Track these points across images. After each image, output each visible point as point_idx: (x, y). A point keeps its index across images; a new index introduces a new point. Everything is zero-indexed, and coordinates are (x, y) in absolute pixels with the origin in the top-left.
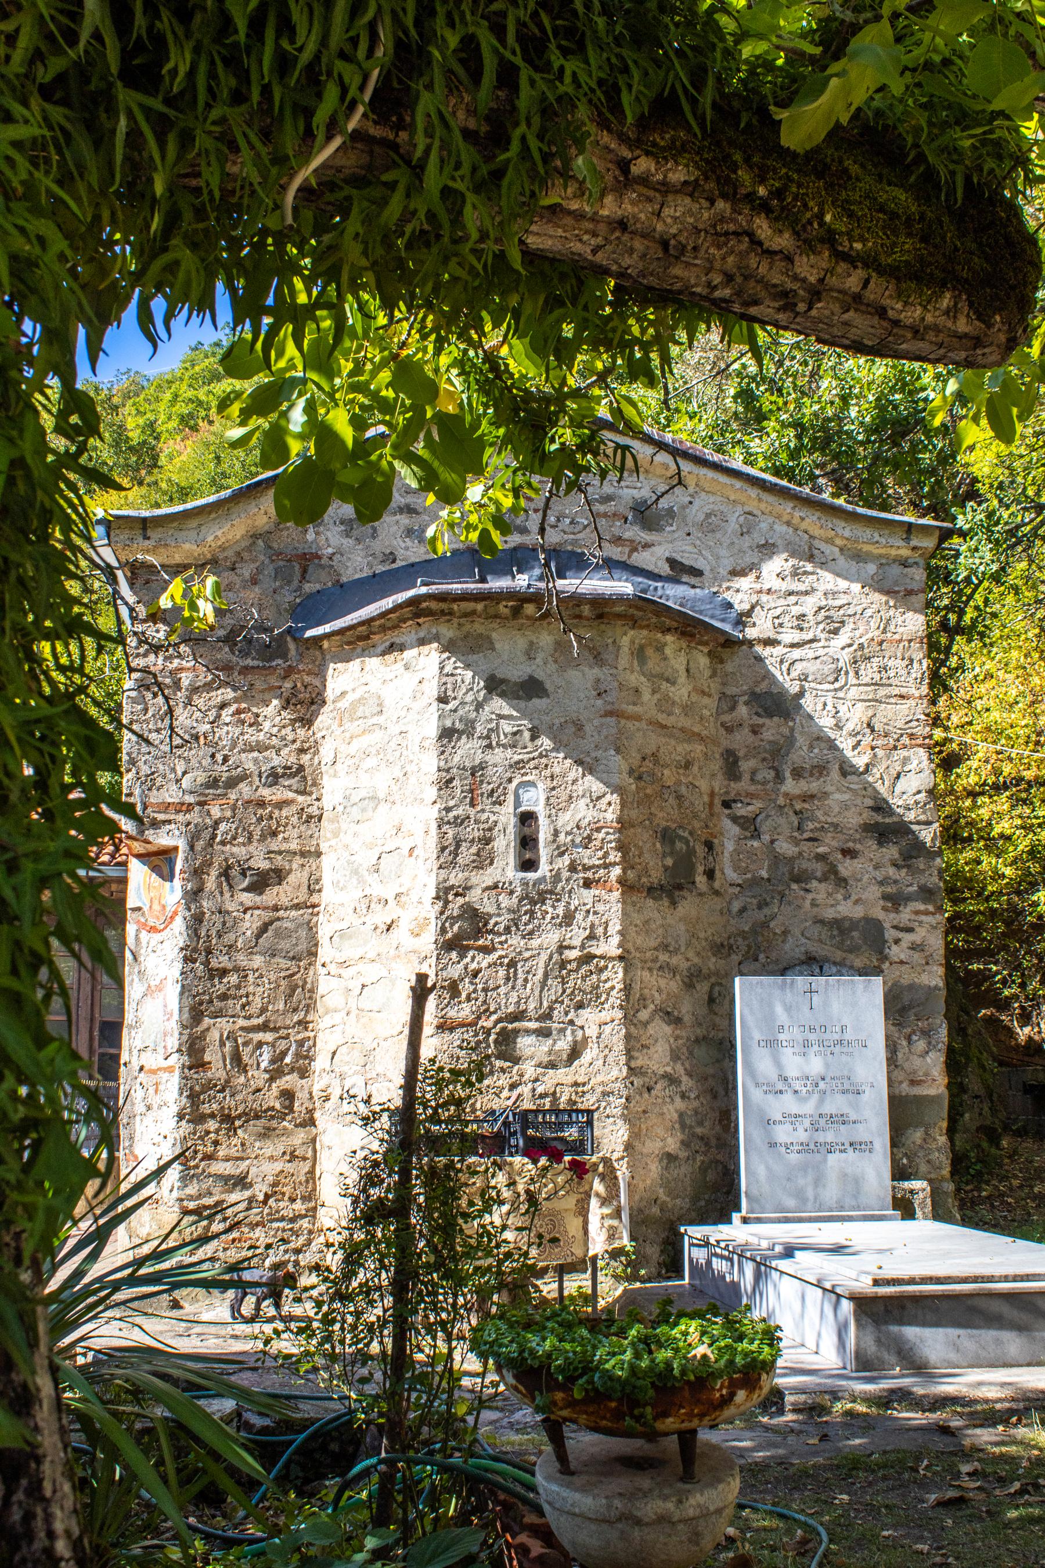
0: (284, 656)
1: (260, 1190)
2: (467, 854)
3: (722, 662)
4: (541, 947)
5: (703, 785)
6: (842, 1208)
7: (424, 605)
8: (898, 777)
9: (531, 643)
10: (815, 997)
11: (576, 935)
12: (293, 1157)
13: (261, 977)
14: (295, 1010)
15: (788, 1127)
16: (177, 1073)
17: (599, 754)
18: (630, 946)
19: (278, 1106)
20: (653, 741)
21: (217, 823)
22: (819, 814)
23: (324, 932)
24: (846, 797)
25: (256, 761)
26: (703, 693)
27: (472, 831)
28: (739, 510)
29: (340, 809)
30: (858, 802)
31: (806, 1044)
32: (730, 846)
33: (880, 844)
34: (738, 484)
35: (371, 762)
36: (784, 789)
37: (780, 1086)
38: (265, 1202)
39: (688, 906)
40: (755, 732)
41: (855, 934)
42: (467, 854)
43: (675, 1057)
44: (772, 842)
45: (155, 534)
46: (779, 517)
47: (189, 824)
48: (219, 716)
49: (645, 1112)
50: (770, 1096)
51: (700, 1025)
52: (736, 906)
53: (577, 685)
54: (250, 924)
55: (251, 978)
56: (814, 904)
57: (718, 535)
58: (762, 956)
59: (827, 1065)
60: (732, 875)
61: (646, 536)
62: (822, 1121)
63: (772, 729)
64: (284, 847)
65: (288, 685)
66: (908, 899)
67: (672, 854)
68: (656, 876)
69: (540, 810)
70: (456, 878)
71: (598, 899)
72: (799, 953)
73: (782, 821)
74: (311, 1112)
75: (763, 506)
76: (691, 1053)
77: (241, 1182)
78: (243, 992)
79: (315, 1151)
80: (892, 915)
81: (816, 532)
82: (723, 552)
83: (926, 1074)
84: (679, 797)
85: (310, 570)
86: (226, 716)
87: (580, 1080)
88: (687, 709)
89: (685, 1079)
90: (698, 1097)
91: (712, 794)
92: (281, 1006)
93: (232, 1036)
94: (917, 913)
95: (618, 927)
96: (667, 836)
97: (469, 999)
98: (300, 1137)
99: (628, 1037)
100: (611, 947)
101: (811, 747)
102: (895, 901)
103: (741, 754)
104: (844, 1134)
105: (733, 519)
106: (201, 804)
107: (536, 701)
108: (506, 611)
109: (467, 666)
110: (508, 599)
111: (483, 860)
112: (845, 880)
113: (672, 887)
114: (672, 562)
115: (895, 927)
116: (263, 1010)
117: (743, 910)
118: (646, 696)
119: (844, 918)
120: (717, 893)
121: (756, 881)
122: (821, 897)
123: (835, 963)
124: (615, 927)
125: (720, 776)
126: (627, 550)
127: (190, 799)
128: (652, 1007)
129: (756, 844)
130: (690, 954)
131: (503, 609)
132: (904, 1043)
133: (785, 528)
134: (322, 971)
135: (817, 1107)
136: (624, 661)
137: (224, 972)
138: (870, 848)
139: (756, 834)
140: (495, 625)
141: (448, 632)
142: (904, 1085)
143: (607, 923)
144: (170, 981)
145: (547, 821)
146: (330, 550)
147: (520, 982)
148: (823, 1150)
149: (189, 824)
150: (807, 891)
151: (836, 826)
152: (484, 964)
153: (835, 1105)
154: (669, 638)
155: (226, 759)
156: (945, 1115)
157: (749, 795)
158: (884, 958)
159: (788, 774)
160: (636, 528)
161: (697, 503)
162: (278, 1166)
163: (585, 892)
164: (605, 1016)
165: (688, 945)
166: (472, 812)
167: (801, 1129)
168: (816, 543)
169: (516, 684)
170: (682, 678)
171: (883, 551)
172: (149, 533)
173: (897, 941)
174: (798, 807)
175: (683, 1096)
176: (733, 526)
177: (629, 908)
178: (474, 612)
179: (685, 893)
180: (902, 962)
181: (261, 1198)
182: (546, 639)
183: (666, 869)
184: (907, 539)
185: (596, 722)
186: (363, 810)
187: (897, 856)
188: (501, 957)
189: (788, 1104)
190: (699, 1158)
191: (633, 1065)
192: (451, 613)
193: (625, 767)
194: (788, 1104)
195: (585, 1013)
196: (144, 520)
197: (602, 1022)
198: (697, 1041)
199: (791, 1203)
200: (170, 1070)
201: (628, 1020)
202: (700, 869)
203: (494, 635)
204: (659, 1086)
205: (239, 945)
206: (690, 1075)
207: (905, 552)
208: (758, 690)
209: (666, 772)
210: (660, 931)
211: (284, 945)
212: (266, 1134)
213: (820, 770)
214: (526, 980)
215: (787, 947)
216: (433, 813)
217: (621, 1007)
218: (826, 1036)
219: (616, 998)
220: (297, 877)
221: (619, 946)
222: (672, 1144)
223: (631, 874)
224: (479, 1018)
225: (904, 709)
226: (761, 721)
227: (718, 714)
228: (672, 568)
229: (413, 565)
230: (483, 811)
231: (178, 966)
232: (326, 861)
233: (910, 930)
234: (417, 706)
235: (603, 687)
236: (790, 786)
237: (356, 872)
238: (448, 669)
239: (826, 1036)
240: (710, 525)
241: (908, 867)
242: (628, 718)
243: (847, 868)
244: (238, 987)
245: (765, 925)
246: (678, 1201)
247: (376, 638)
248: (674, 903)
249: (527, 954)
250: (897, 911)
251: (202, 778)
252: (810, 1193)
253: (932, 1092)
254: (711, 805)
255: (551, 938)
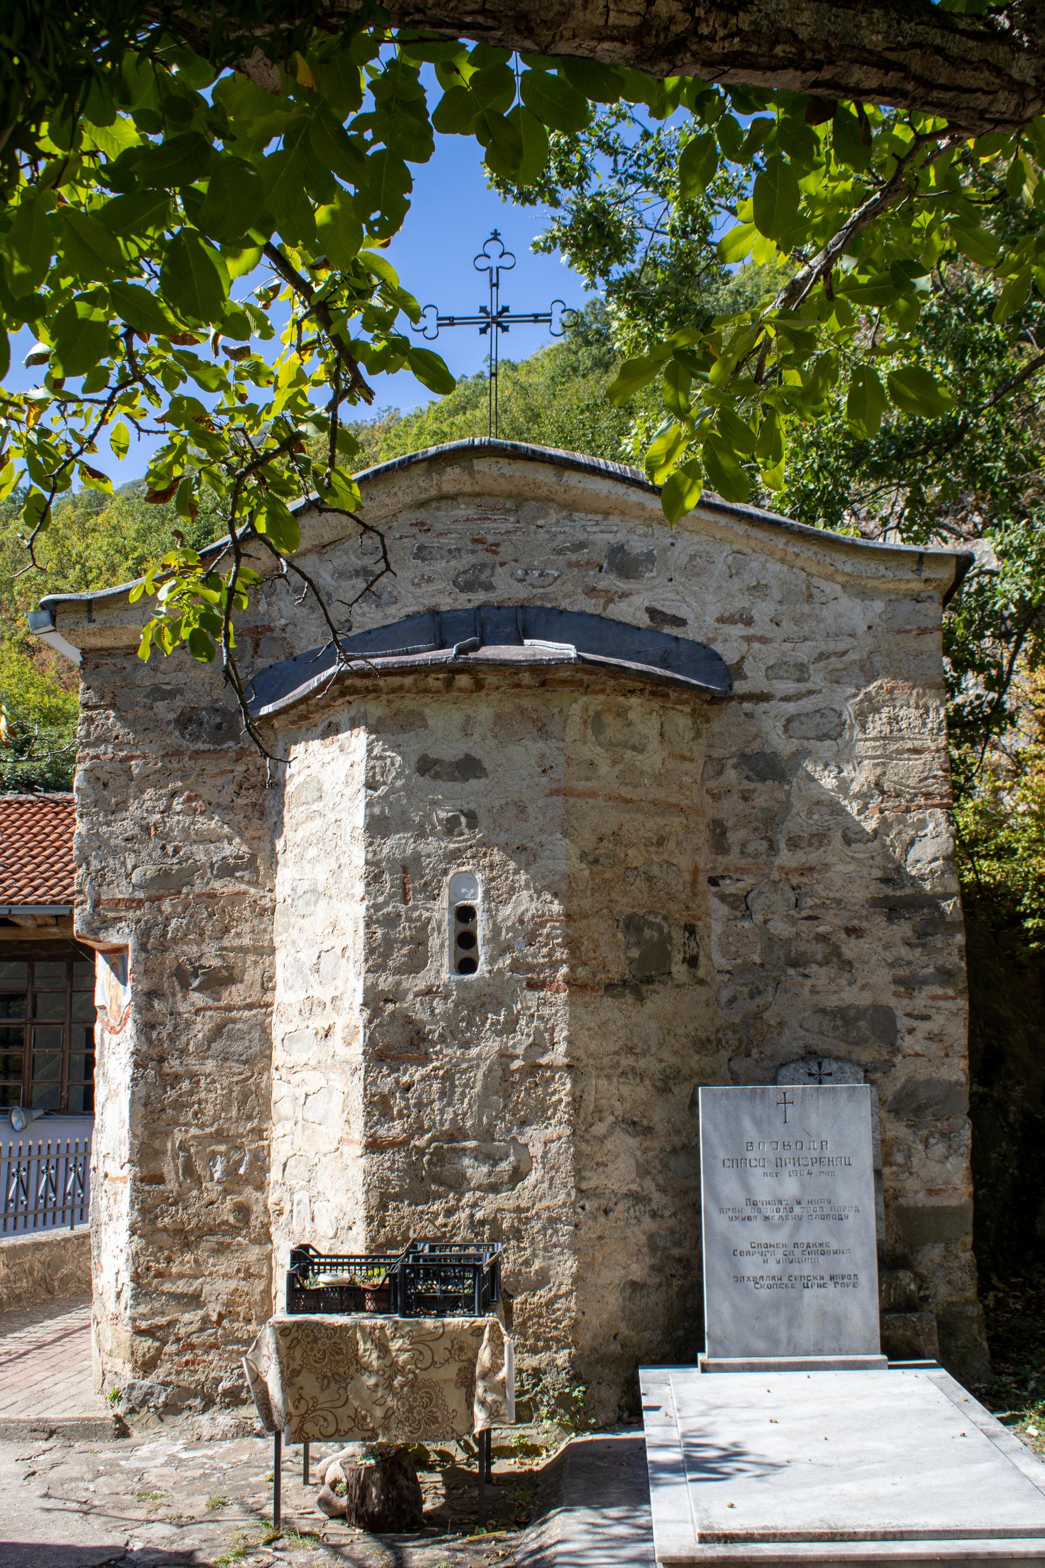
0: (236, 738)
1: (213, 1310)
2: (399, 955)
3: (708, 721)
4: (479, 1056)
5: (684, 862)
6: (820, 1352)
7: (348, 682)
8: (912, 843)
9: (468, 717)
10: (790, 1109)
11: (520, 1041)
12: (249, 1276)
13: (213, 1084)
14: (249, 1118)
15: (757, 1258)
16: (129, 1184)
17: (544, 838)
18: (581, 1053)
19: (232, 1220)
20: (614, 818)
21: (168, 919)
22: (819, 888)
23: (277, 1033)
24: (851, 868)
25: (207, 852)
26: (683, 758)
27: (404, 930)
28: (727, 548)
29: (289, 901)
30: (865, 873)
31: (779, 1163)
32: (717, 928)
33: (890, 920)
34: (723, 520)
35: (312, 852)
36: (778, 861)
37: (748, 1211)
38: (219, 1322)
39: (661, 1000)
40: (745, 799)
41: (862, 1024)
42: (399, 955)
43: (643, 1171)
44: (766, 922)
45: (99, 616)
46: (771, 554)
47: (138, 921)
48: (169, 808)
49: (600, 1238)
50: (736, 1224)
51: (678, 1132)
52: (725, 995)
53: (517, 763)
54: (201, 1028)
55: (202, 1084)
56: (814, 991)
57: (704, 579)
58: (754, 1052)
59: (803, 1187)
60: (720, 961)
61: (623, 585)
62: (797, 1252)
63: (765, 795)
64: (237, 942)
65: (240, 768)
66: (924, 982)
67: (638, 944)
68: (617, 970)
69: (478, 902)
70: (386, 982)
71: (545, 1002)
72: (797, 1047)
73: (777, 898)
74: (266, 1226)
75: (753, 543)
76: (665, 1165)
77: (194, 1300)
78: (195, 1098)
79: (271, 1269)
80: (905, 1002)
81: (814, 569)
82: (710, 598)
83: (947, 1182)
84: (649, 878)
85: (262, 643)
86: (177, 805)
87: (523, 1205)
88: (660, 778)
89: (656, 1196)
90: (675, 1214)
91: (696, 871)
92: (234, 1113)
93: (183, 1147)
94: (934, 998)
95: (565, 1033)
96: (632, 925)
97: (401, 1116)
98: (254, 1253)
99: (577, 1157)
100: (558, 1055)
101: (810, 813)
102: (908, 985)
103: (729, 824)
104: (824, 1265)
105: (720, 560)
106: (152, 900)
107: (473, 782)
108: (439, 684)
109: (396, 747)
110: (439, 671)
111: (416, 963)
112: (850, 963)
113: (637, 984)
114: (652, 612)
115: (909, 1015)
116: (216, 1118)
117: (733, 1000)
118: (604, 769)
119: (849, 1007)
120: (701, 982)
121: (748, 967)
122: (821, 982)
123: (837, 1059)
124: (561, 1034)
125: (706, 850)
126: (602, 601)
127: (140, 895)
128: (611, 1119)
129: (747, 925)
130: (665, 1054)
131: (432, 681)
132: (920, 1147)
133: (778, 566)
134: (275, 1075)
135: (792, 1235)
136: (573, 731)
137: (177, 1078)
138: (878, 925)
139: (748, 913)
140: (428, 700)
141: (375, 709)
142: (921, 1195)
143: (553, 1028)
144: (123, 1087)
145: (485, 916)
146: (283, 622)
147: (456, 1096)
148: (798, 1285)
149: (138, 921)
150: (806, 976)
151: (838, 902)
152: (417, 1077)
153: (814, 1232)
154: (634, 701)
155: (176, 851)
156: (969, 1228)
157: (737, 869)
158: (895, 1050)
159: (782, 845)
160: (612, 577)
161: (680, 543)
162: (232, 1284)
163: (529, 994)
164: (552, 1132)
165: (661, 1044)
166: (402, 908)
167: (772, 1262)
168: (815, 581)
169: (450, 764)
170: (654, 744)
171: (891, 586)
172: (95, 615)
173: (911, 1031)
174: (795, 882)
175: (654, 1215)
176: (720, 567)
177: (580, 1011)
178: (401, 688)
179: (656, 986)
180: (917, 1055)
181: (214, 1318)
182: (484, 711)
183: (631, 961)
184: (919, 570)
185: (541, 803)
186: (308, 904)
187: (910, 933)
188: (435, 1069)
189: (759, 1232)
190: (676, 1283)
191: (584, 1186)
192: (376, 690)
193: (574, 851)
194: (759, 1232)
195: (529, 1131)
196: (89, 602)
197: (546, 1138)
198: (674, 1150)
199: (761, 1345)
200: (123, 1179)
201: (577, 1135)
202: (678, 957)
203: (427, 711)
204: (620, 1207)
205: (191, 1048)
206: (663, 1190)
207: (916, 586)
208: (748, 751)
209: (631, 852)
210: (622, 1033)
211: (237, 1047)
212: (221, 1249)
213: (820, 838)
214: (463, 1095)
215: (784, 1040)
216: (360, 910)
217: (569, 1122)
218: (805, 1153)
219: (563, 1113)
220: (253, 975)
221: (567, 1054)
222: (638, 1271)
223: (582, 972)
224: (411, 1137)
225: (917, 763)
226: (751, 786)
227: (703, 780)
228: (652, 619)
229: (369, 632)
230: (416, 908)
231: (130, 1071)
232: (280, 957)
233: (926, 1018)
234: (349, 791)
235: (548, 763)
236: (785, 858)
237: (300, 971)
238: (376, 751)
239: (805, 1153)
240: (694, 568)
241: (924, 945)
242: (580, 795)
243: (851, 948)
244: (191, 1093)
245: (758, 1016)
246: (647, 1334)
247: (316, 717)
248: (640, 998)
249: (464, 1066)
250: (911, 997)
251: (151, 870)
252: (783, 1334)
253: (953, 1202)
254: (694, 883)
255: (490, 1046)
